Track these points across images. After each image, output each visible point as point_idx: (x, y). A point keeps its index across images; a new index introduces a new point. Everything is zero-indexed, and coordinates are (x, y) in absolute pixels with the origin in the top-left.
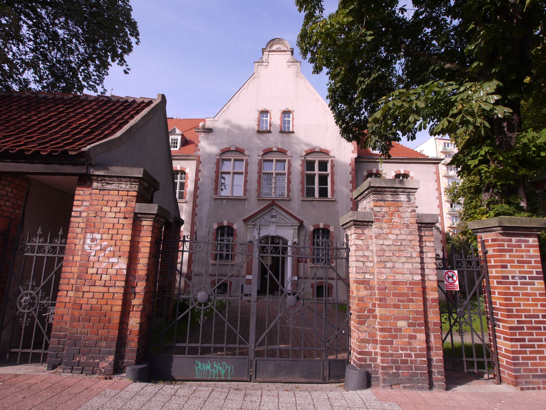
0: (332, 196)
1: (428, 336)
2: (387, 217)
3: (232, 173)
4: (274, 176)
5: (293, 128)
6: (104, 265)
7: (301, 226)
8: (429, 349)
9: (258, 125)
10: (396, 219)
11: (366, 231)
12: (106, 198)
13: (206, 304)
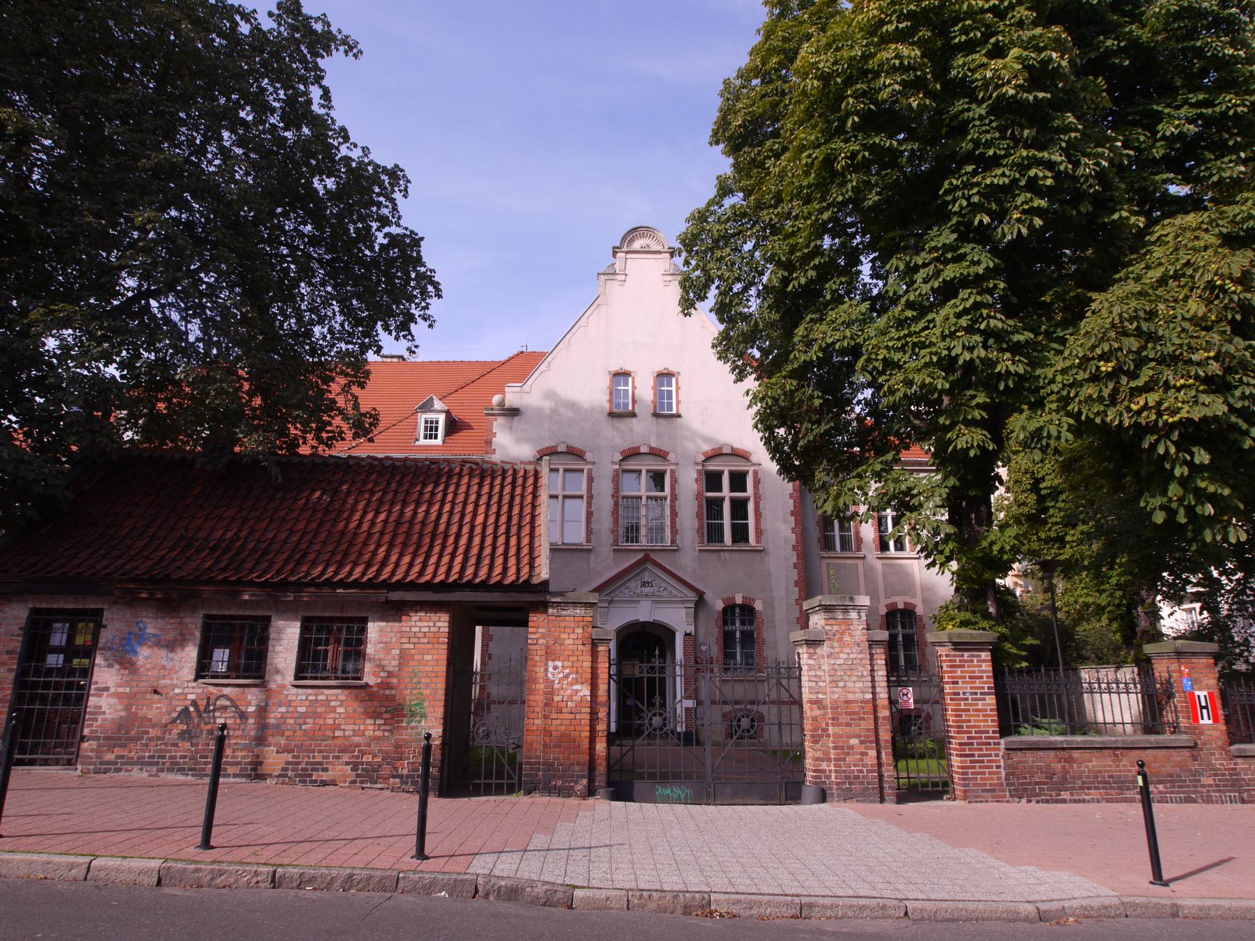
0: (758, 540)
1: (879, 753)
3: (560, 498)
4: (644, 502)
6: (568, 692)
7: (700, 602)
8: (880, 765)
9: (610, 401)
10: (847, 638)
11: (818, 650)
12: (563, 624)
13: (661, 729)
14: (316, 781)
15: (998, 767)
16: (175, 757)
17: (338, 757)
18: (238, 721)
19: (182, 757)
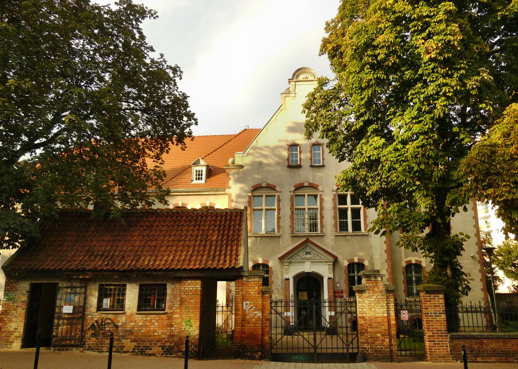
2: (372, 288)
5: (323, 161)
6: (252, 315)
7: (336, 262)
11: (363, 295)
14: (147, 354)
15: (447, 346)
16: (90, 344)
17: (156, 344)
18: (115, 329)
19: (92, 344)
